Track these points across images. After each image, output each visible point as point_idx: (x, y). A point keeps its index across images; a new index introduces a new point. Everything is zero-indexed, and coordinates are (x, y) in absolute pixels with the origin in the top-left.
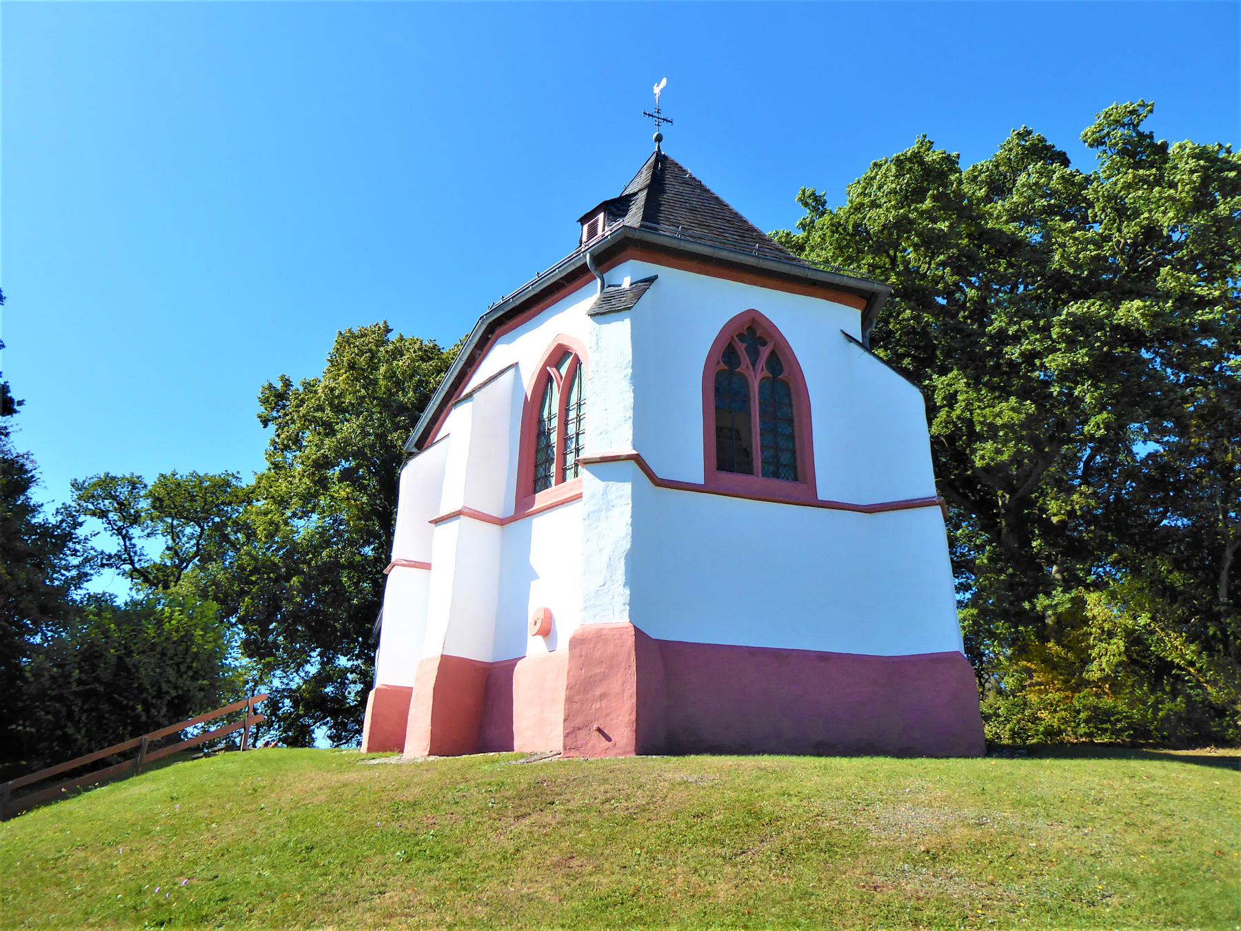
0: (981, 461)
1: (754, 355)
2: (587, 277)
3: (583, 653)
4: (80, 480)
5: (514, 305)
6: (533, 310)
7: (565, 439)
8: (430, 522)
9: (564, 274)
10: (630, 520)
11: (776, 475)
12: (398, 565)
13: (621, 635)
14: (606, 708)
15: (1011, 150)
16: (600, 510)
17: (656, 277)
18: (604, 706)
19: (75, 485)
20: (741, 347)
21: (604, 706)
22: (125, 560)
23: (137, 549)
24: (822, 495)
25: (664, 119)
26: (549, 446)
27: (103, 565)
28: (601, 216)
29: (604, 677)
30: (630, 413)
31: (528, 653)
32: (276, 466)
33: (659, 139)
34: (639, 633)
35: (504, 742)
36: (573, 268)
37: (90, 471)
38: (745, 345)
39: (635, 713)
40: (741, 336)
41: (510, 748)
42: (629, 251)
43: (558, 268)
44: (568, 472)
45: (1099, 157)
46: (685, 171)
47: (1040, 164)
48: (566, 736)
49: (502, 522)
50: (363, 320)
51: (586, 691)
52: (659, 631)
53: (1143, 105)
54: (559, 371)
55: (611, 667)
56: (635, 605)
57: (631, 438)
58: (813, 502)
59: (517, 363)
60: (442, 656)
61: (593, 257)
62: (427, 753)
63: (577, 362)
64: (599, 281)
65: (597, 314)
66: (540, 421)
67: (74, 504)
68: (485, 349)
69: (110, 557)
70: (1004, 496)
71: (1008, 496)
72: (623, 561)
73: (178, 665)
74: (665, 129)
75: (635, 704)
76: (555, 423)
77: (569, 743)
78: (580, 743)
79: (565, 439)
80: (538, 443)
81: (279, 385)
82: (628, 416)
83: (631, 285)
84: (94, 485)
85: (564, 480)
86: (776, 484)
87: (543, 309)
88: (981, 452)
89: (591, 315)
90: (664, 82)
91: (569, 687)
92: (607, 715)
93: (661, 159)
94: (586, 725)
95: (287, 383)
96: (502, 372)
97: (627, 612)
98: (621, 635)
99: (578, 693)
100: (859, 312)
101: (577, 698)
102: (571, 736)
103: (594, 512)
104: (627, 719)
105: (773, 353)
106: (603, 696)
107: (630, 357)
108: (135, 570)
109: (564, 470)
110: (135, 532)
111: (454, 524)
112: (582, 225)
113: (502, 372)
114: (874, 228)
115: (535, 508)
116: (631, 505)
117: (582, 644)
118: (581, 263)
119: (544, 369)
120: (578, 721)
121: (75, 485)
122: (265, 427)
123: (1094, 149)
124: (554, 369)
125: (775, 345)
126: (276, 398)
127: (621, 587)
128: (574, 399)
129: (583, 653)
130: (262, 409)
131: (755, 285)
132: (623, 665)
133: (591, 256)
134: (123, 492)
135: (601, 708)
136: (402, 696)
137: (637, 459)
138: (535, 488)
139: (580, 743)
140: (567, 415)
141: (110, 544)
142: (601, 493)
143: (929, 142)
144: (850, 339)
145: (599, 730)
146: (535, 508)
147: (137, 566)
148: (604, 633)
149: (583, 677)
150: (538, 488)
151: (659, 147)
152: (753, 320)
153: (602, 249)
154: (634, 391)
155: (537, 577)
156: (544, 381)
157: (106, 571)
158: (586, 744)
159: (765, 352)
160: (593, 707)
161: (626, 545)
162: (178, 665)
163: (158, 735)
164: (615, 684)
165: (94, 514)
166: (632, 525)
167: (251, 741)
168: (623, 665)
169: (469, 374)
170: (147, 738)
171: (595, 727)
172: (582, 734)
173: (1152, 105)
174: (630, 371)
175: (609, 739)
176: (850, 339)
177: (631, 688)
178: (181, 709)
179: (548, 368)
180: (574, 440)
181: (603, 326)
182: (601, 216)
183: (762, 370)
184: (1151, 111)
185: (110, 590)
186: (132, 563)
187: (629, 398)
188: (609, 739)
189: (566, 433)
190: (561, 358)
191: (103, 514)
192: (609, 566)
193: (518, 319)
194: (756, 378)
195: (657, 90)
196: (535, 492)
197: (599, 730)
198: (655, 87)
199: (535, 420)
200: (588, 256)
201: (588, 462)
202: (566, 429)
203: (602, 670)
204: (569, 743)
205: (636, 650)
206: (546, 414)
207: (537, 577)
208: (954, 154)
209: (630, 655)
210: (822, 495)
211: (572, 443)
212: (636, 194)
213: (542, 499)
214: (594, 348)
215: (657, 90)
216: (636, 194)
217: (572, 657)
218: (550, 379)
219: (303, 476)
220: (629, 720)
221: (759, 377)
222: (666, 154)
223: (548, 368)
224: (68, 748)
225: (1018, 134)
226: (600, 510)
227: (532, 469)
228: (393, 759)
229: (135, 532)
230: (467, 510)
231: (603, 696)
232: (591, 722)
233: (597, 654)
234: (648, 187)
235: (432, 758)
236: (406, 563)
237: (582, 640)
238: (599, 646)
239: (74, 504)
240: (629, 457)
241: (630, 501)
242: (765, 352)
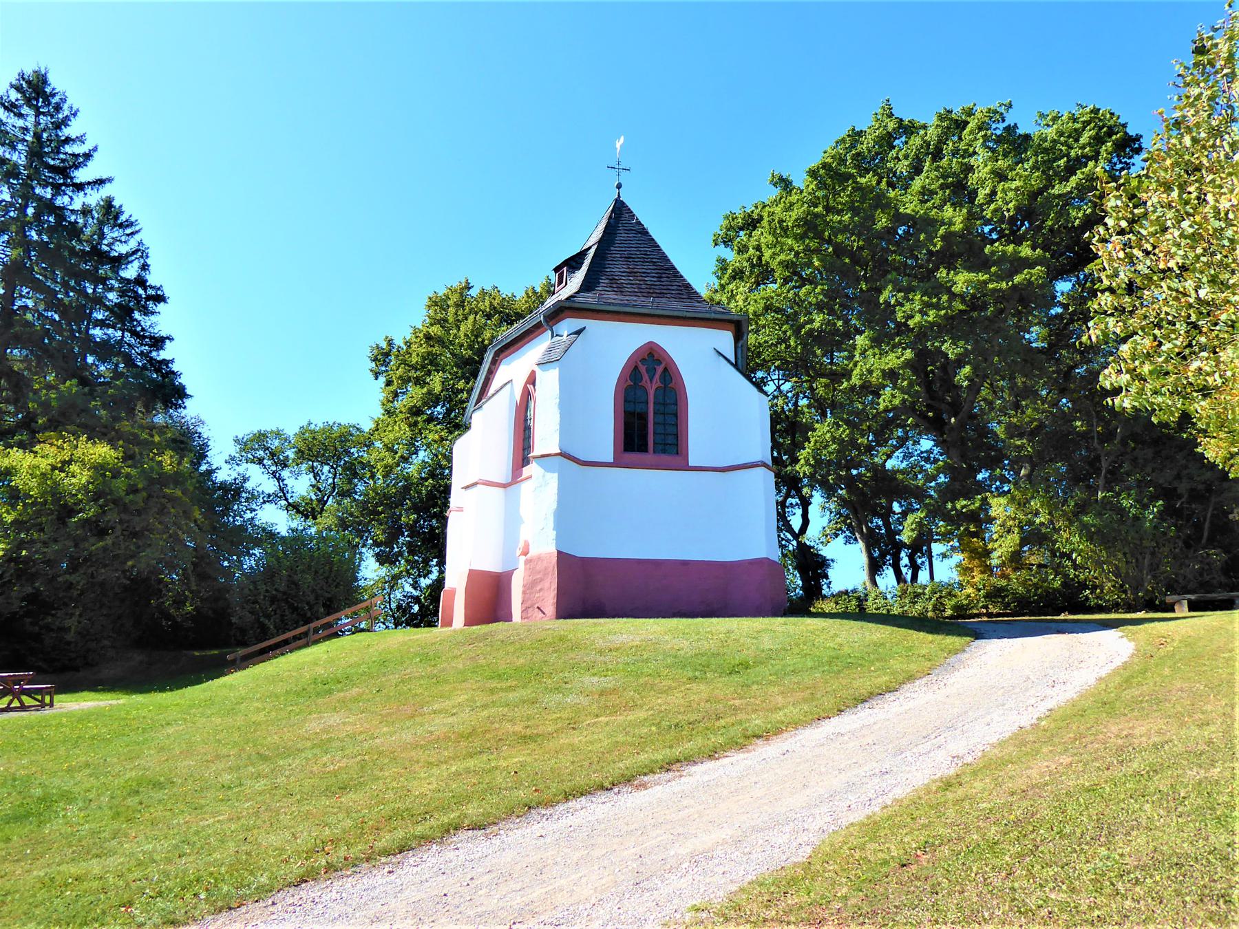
1: (651, 372)
4: (240, 437)
11: (664, 451)
19: (237, 441)
20: (643, 369)
22: (281, 497)
23: (289, 488)
24: (692, 463)
27: (264, 502)
29: (541, 580)
32: (389, 413)
33: (619, 186)
34: (559, 553)
37: (246, 429)
40: (643, 360)
49: (504, 486)
51: (532, 588)
55: (545, 575)
60: (471, 571)
61: (544, 317)
67: (237, 455)
69: (269, 496)
73: (327, 578)
77: (524, 616)
81: (384, 345)
84: (252, 441)
86: (665, 458)
91: (524, 586)
93: (620, 211)
94: (532, 606)
95: (390, 342)
96: (502, 388)
105: (666, 369)
106: (541, 590)
108: (290, 504)
110: (285, 473)
113: (502, 388)
115: (523, 477)
119: (525, 385)
121: (237, 441)
126: (382, 357)
130: (373, 365)
134: (275, 444)
136: (453, 591)
141: (270, 486)
146: (523, 477)
147: (290, 501)
152: (651, 349)
157: (267, 506)
161: (554, 506)
162: (327, 578)
163: (317, 623)
164: (546, 584)
165: (252, 462)
167: (876, 727)
170: (312, 625)
174: (558, 400)
177: (555, 586)
178: (332, 607)
185: (271, 521)
186: (286, 500)
191: (260, 461)
193: (512, 349)
194: (652, 387)
201: (535, 458)
204: (524, 616)
210: (692, 463)
221: (654, 387)
224: (264, 634)
229: (285, 473)
231: (541, 590)
239: (237, 455)
242: (660, 370)
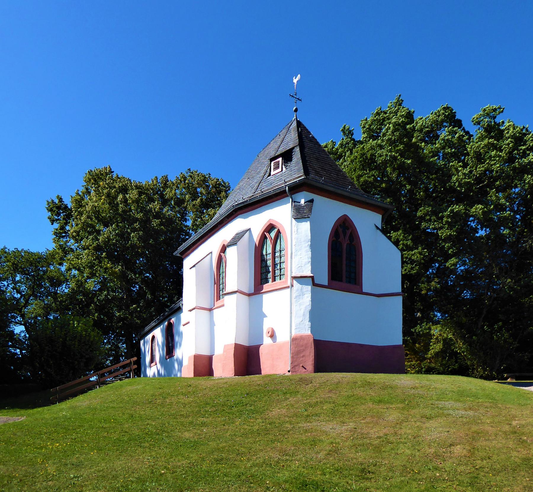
0: (405, 272)
3: (297, 343)
7: (274, 265)
11: (350, 282)
13: (309, 337)
15: (439, 116)
16: (300, 295)
20: (340, 230)
21: (304, 359)
25: (298, 99)
26: (267, 266)
28: (280, 159)
29: (304, 350)
30: (310, 260)
31: (264, 343)
35: (258, 371)
36: (279, 191)
38: (342, 229)
40: (340, 225)
41: (260, 373)
44: (276, 277)
45: (476, 131)
46: (309, 132)
47: (451, 127)
49: (249, 295)
50: (99, 166)
52: (317, 338)
53: (500, 108)
54: (270, 234)
55: (306, 347)
57: (310, 270)
58: (361, 292)
59: (250, 229)
63: (279, 232)
66: (262, 255)
68: (230, 219)
70: (407, 284)
71: (409, 284)
72: (308, 313)
74: (299, 105)
76: (270, 257)
79: (274, 265)
80: (261, 264)
83: (305, 203)
85: (275, 280)
88: (406, 268)
98: (309, 337)
100: (381, 216)
103: (298, 296)
105: (351, 233)
106: (303, 356)
107: (310, 238)
109: (275, 277)
111: (235, 296)
112: (271, 161)
114: (379, 160)
116: (310, 294)
120: (296, 364)
122: (52, 224)
123: (475, 126)
127: (308, 322)
128: (278, 248)
129: (297, 343)
131: (347, 203)
133: (288, 188)
135: (303, 360)
137: (312, 278)
138: (261, 283)
140: (275, 254)
142: (300, 289)
143: (402, 100)
144: (377, 228)
145: (302, 366)
148: (303, 336)
150: (262, 283)
153: (294, 185)
155: (266, 316)
156: (263, 238)
158: (298, 370)
159: (348, 232)
161: (309, 308)
169: (219, 227)
171: (301, 365)
172: (297, 367)
173: (504, 109)
174: (310, 243)
175: (305, 369)
176: (377, 228)
179: (265, 233)
180: (279, 265)
183: (347, 241)
184: (502, 111)
187: (309, 254)
188: (305, 369)
189: (275, 262)
190: (271, 229)
192: (304, 315)
195: (295, 81)
197: (302, 366)
199: (260, 255)
200: (287, 187)
202: (275, 260)
206: (264, 253)
207: (266, 316)
208: (412, 110)
209: (311, 345)
211: (277, 266)
212: (293, 148)
213: (266, 287)
214: (296, 233)
215: (295, 81)
218: (266, 238)
219: (89, 255)
222: (300, 121)
223: (265, 233)
225: (444, 108)
226: (300, 295)
231: (303, 356)
232: (300, 364)
233: (301, 343)
237: (296, 339)
238: (302, 341)
240: (310, 277)
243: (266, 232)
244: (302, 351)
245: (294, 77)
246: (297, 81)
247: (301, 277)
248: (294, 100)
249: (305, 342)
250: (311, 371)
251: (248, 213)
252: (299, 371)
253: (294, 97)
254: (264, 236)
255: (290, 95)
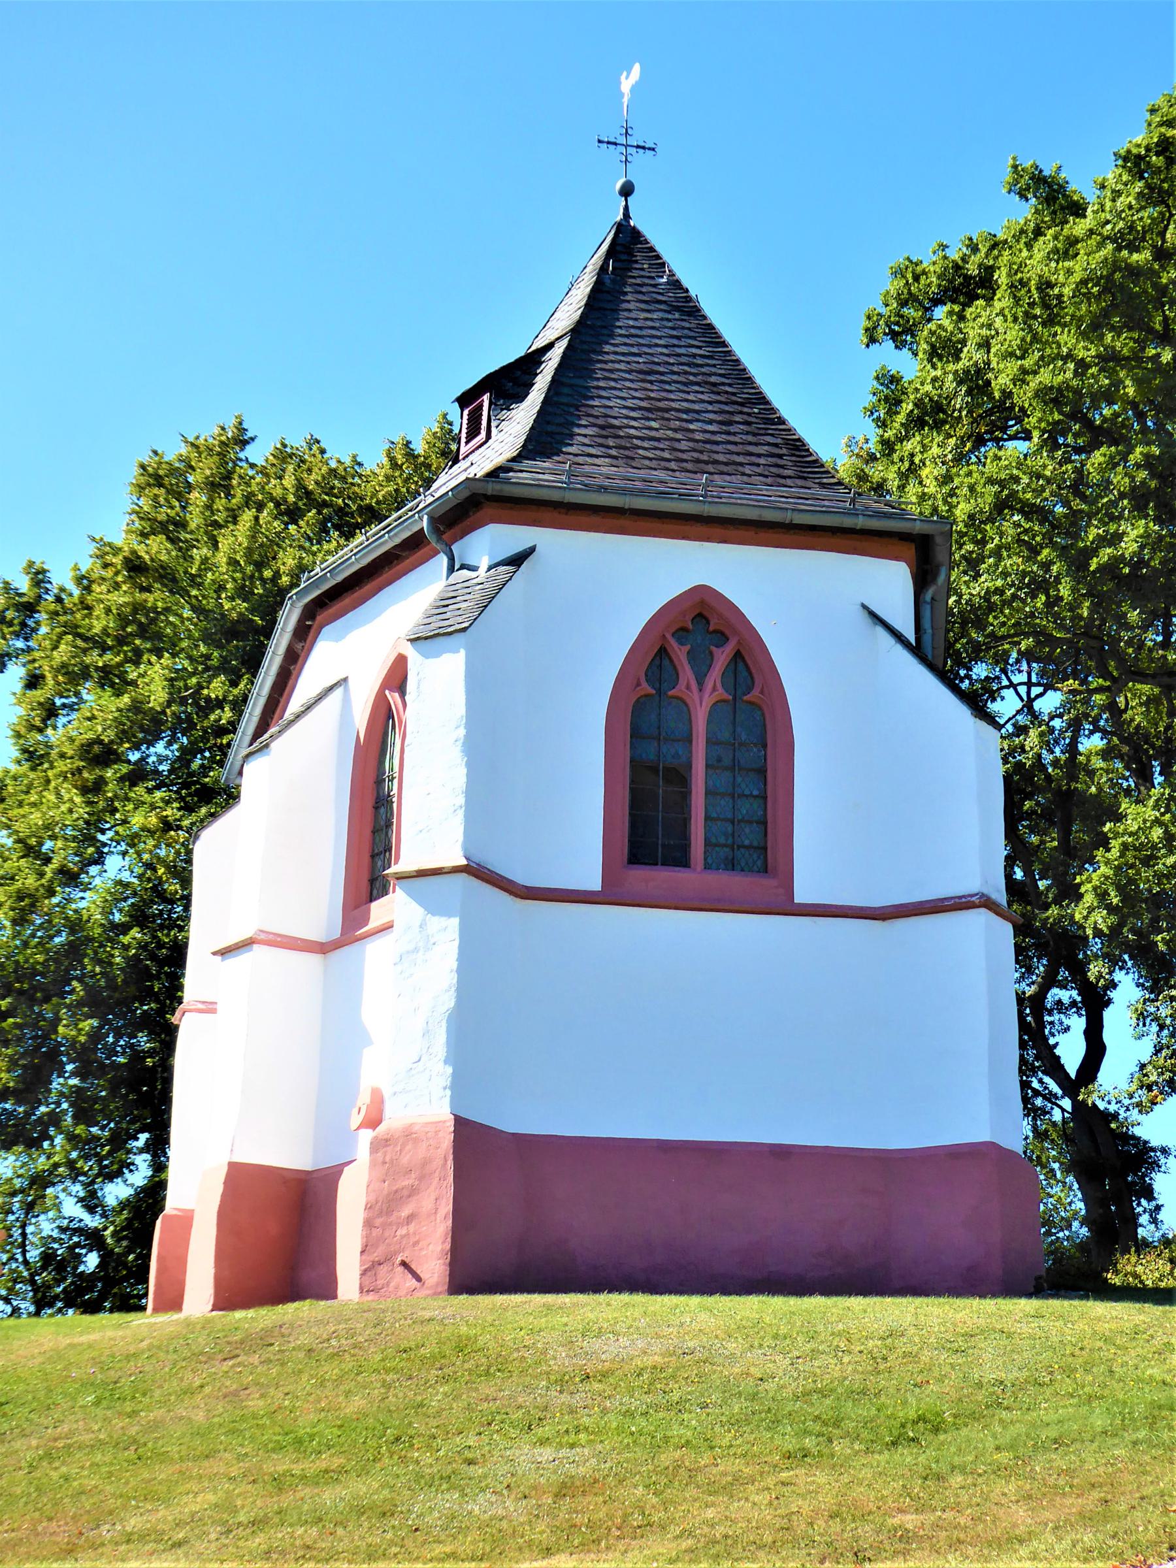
2: (424, 551)
3: (388, 1159)
5: (332, 583)
6: (368, 587)
8: (214, 954)
9: (397, 541)
10: (455, 965)
11: (731, 865)
12: (190, 1011)
14: (414, 1234)
17: (531, 551)
18: (411, 1231)
20: (680, 653)
21: (411, 1231)
24: (803, 894)
25: (638, 147)
29: (413, 1192)
30: (461, 800)
33: (627, 191)
39: (449, 1240)
40: (682, 633)
41: (335, 1297)
42: (488, 510)
43: (388, 532)
48: (364, 1273)
49: (323, 948)
51: (389, 1212)
55: (421, 1178)
56: (458, 1086)
57: (461, 838)
58: (788, 907)
59: (345, 680)
61: (432, 520)
62: (210, 1307)
64: (443, 560)
65: (418, 639)
72: (444, 1024)
74: (641, 169)
75: (450, 1228)
78: (380, 1282)
81: (23, 584)
82: (458, 804)
87: (380, 589)
89: (411, 640)
90: (637, 68)
91: (369, 1207)
92: (416, 1243)
95: (39, 577)
96: (331, 689)
97: (448, 1100)
98: (437, 1132)
99: (380, 1214)
101: (378, 1222)
102: (369, 1274)
103: (408, 952)
104: (439, 1248)
105: (738, 656)
106: (410, 1218)
107: (461, 710)
113: (331, 689)
116: (457, 943)
117: (386, 1146)
118: (416, 529)
120: (376, 1256)
124: (396, 695)
125: (739, 642)
127: (442, 1063)
129: (388, 1159)
132: (437, 1174)
135: (408, 1235)
137: (475, 870)
139: (380, 1282)
145: (404, 1264)
148: (416, 1128)
149: (385, 1192)
150: (375, 892)
151: (626, 208)
152: (703, 603)
154: (468, 765)
158: (388, 1284)
160: (398, 1233)
164: (425, 1201)
166: (459, 971)
168: (437, 1174)
169: (294, 673)
172: (382, 1270)
174: (462, 732)
177: (447, 1207)
179: (387, 692)
181: (431, 660)
182: (486, 398)
183: (714, 689)
192: (426, 1033)
193: (347, 601)
196: (372, 899)
197: (404, 1264)
198: (623, 77)
200: (426, 517)
203: (411, 1182)
205: (454, 1153)
209: (446, 1161)
210: (803, 894)
216: (550, 346)
217: (373, 1164)
220: (442, 1250)
221: (708, 700)
223: (387, 692)
227: (366, 859)
228: (176, 1316)
230: (262, 936)
231: (410, 1218)
232: (396, 1253)
233: (405, 1160)
234: (572, 330)
235: (214, 1313)
236: (201, 1006)
237: (387, 1140)
238: (408, 1147)
240: (456, 870)
241: (456, 936)
243: (391, 690)
244: (405, 1193)
245: (625, 74)
246: (634, 89)
247: (422, 874)
248: (615, 153)
249: (422, 1152)
250: (437, 1284)
251: (349, 615)
252: (392, 1285)
253: (616, 144)
254: (384, 711)
255: (600, 141)
